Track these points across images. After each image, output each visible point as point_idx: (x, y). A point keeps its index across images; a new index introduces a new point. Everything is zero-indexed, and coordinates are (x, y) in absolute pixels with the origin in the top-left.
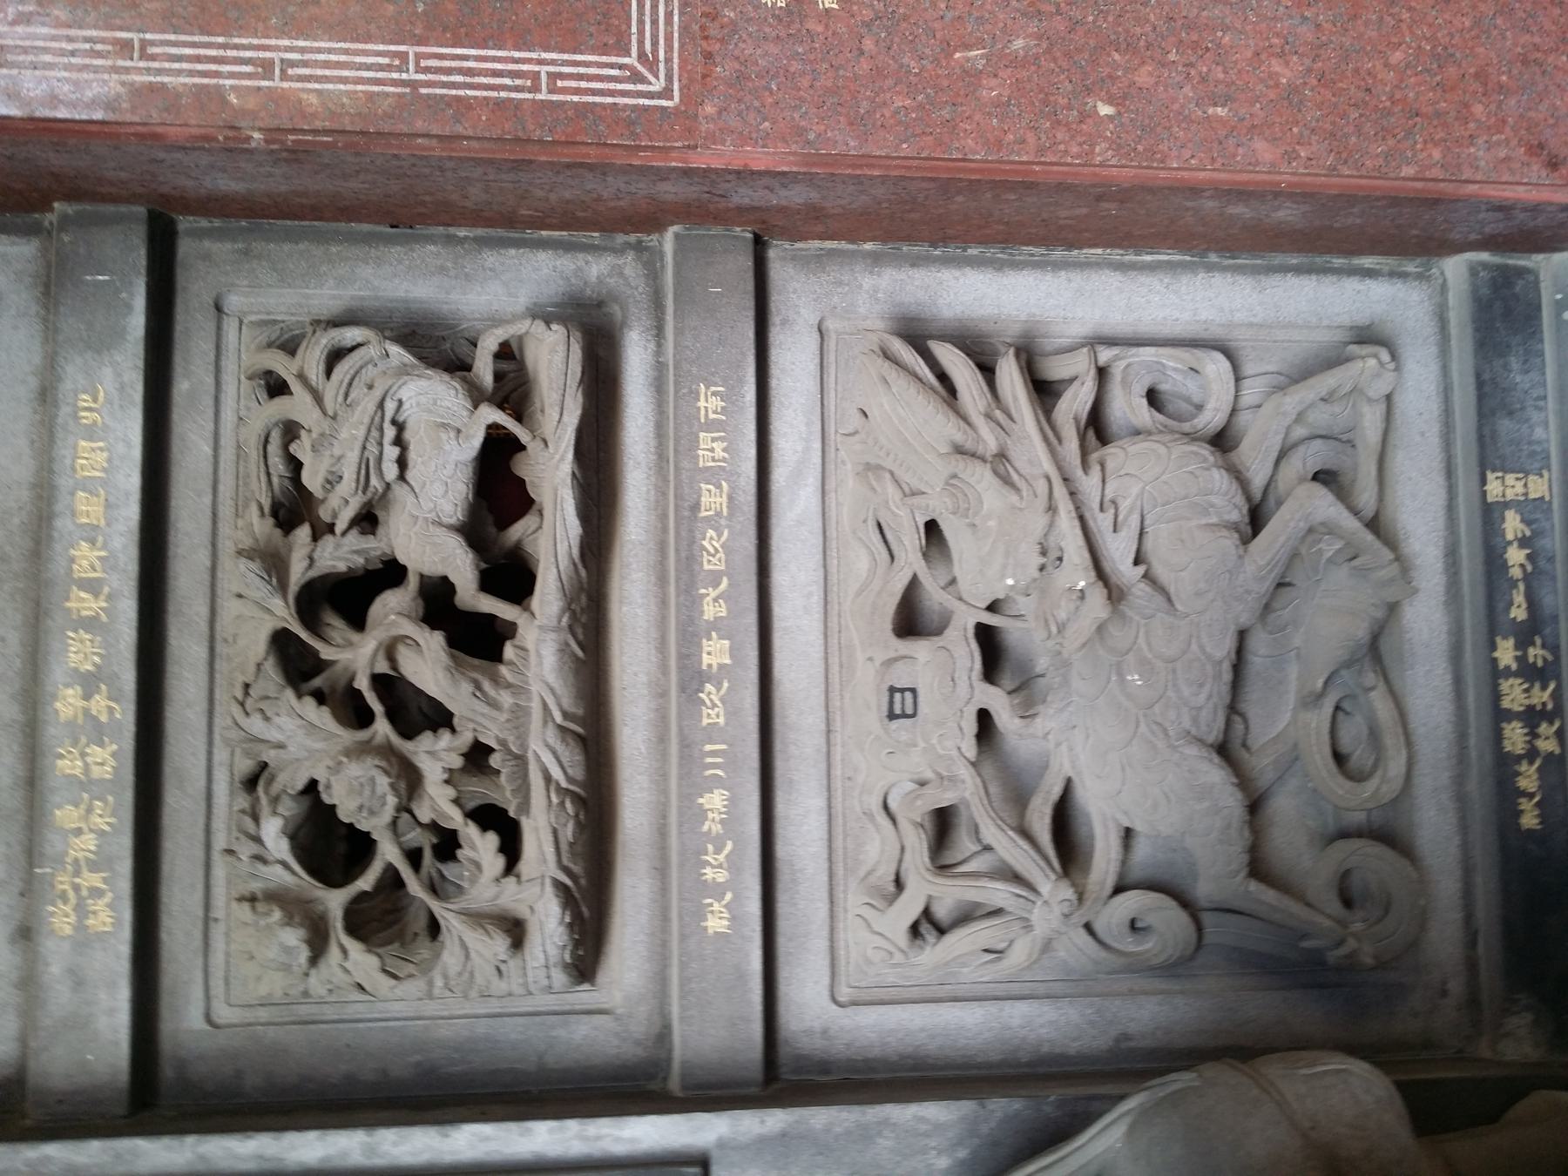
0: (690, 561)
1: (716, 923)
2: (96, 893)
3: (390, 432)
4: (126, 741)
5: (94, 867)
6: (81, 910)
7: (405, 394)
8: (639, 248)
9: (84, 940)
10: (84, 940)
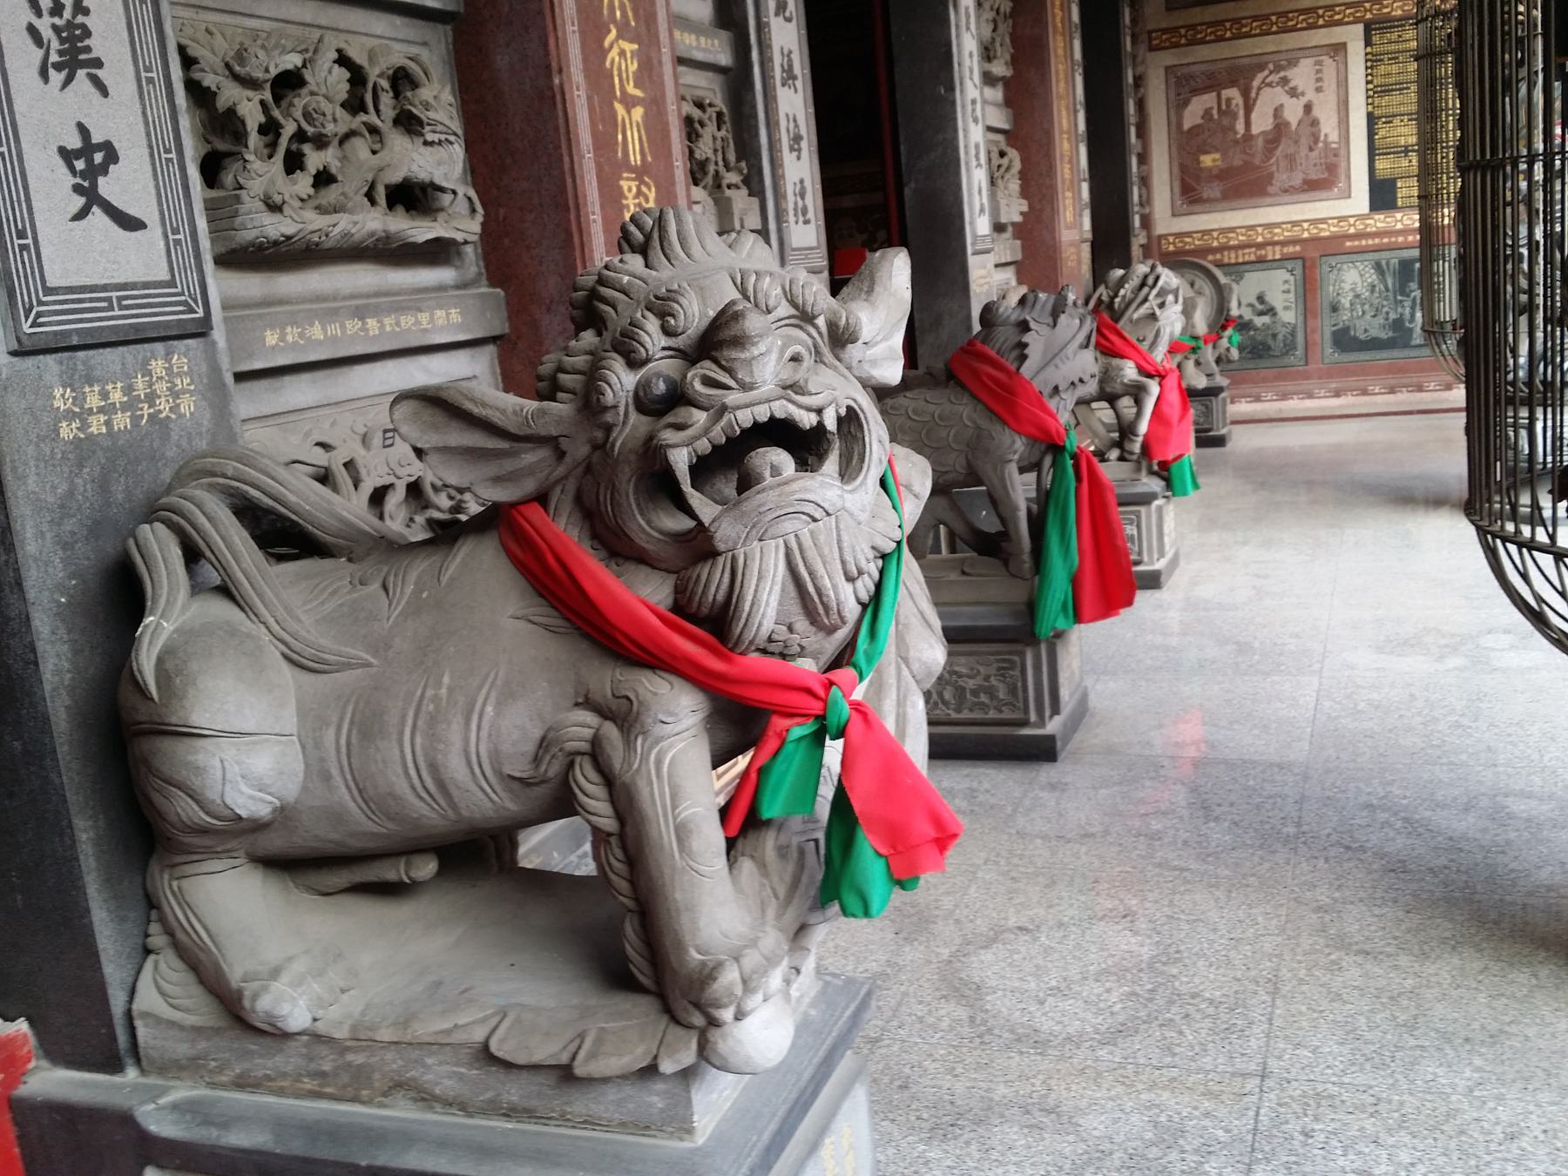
0: (377, 311)
1: (271, 338)
3: (443, 137)
7: (456, 146)
8: (480, 274)
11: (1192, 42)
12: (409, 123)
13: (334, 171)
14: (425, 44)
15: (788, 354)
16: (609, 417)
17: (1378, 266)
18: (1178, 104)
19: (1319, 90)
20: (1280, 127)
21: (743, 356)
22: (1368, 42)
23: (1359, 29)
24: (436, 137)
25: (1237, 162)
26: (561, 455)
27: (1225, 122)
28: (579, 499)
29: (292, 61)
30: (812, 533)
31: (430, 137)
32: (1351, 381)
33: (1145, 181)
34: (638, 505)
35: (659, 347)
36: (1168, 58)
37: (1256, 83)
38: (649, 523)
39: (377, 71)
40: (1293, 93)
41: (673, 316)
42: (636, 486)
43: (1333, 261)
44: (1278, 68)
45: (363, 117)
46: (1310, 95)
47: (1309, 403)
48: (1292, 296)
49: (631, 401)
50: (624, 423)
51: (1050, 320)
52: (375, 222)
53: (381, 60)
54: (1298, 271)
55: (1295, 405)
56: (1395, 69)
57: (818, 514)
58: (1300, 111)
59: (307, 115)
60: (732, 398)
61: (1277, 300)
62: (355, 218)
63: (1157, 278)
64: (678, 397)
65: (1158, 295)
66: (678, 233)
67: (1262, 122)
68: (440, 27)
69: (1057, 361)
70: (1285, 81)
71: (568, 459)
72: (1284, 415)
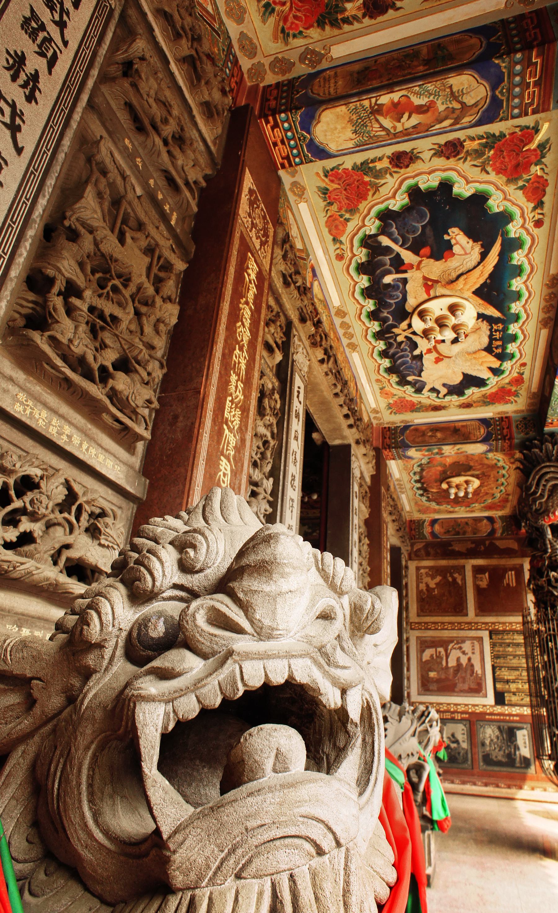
2: (25, 410)
3: (111, 545)
4: (55, 438)
5: (31, 413)
6: (22, 403)
9: (15, 399)
10: (15, 399)
11: (426, 629)
12: (93, 532)
13: (36, 535)
14: (120, 508)
15: (319, 608)
16: (91, 660)
17: (499, 728)
18: (421, 651)
19: (473, 653)
20: (459, 665)
21: (267, 588)
22: (491, 638)
23: (487, 633)
24: (107, 543)
25: (443, 677)
26: (30, 703)
27: (439, 660)
28: (33, 768)
29: (35, 472)
30: (314, 875)
31: (103, 542)
32: (492, 780)
33: (408, 679)
34: (90, 786)
35: (168, 582)
36: (417, 633)
37: (450, 647)
38: (96, 816)
39: (85, 499)
40: (464, 653)
41: (194, 547)
42: (95, 757)
43: (482, 723)
44: (458, 643)
45: (66, 515)
46: (470, 655)
47: (474, 788)
48: (465, 736)
49: (121, 643)
50: (106, 669)
51: (398, 718)
52: (51, 573)
53: (89, 494)
54: (468, 726)
55: (468, 788)
56: (501, 649)
57: (327, 843)
58: (466, 661)
59: (32, 502)
60: (241, 644)
61: (460, 737)
62: (39, 565)
63: (429, 713)
64: (178, 637)
65: (429, 721)
66: (222, 502)
67: (452, 663)
68: (132, 504)
69: (401, 741)
70: (460, 648)
71: (37, 710)
72: (464, 792)
